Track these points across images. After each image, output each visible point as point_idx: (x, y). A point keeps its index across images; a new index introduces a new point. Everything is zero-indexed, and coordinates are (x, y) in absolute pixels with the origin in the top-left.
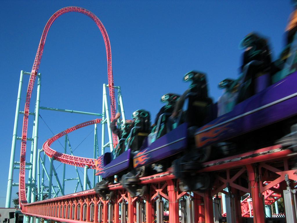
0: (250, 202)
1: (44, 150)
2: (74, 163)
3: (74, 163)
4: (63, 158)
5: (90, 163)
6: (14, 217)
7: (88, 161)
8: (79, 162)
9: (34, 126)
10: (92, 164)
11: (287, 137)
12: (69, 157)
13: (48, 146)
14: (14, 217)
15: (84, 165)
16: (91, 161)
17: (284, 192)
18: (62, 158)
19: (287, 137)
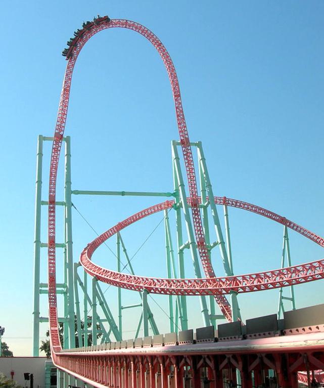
0: (51, 326)
1: (81, 263)
2: (159, 289)
3: (159, 289)
4: (102, 275)
5: (150, 285)
6: (218, 326)
7: (162, 284)
8: (133, 283)
9: (181, 208)
10: (152, 286)
11: (120, 317)
12: (119, 275)
13: (88, 259)
14: (218, 326)
15: (141, 287)
16: (152, 281)
17: (217, 314)
18: (108, 278)
19: (120, 317)
